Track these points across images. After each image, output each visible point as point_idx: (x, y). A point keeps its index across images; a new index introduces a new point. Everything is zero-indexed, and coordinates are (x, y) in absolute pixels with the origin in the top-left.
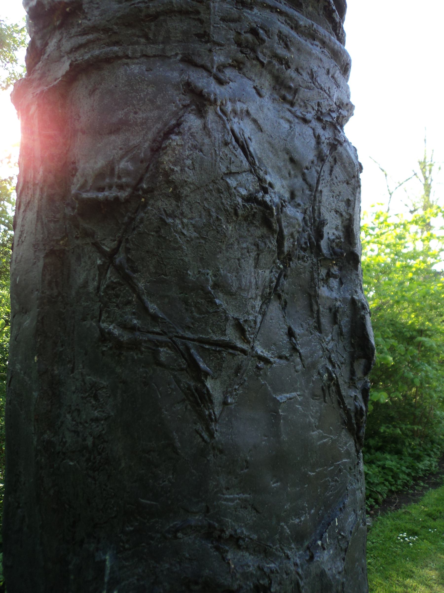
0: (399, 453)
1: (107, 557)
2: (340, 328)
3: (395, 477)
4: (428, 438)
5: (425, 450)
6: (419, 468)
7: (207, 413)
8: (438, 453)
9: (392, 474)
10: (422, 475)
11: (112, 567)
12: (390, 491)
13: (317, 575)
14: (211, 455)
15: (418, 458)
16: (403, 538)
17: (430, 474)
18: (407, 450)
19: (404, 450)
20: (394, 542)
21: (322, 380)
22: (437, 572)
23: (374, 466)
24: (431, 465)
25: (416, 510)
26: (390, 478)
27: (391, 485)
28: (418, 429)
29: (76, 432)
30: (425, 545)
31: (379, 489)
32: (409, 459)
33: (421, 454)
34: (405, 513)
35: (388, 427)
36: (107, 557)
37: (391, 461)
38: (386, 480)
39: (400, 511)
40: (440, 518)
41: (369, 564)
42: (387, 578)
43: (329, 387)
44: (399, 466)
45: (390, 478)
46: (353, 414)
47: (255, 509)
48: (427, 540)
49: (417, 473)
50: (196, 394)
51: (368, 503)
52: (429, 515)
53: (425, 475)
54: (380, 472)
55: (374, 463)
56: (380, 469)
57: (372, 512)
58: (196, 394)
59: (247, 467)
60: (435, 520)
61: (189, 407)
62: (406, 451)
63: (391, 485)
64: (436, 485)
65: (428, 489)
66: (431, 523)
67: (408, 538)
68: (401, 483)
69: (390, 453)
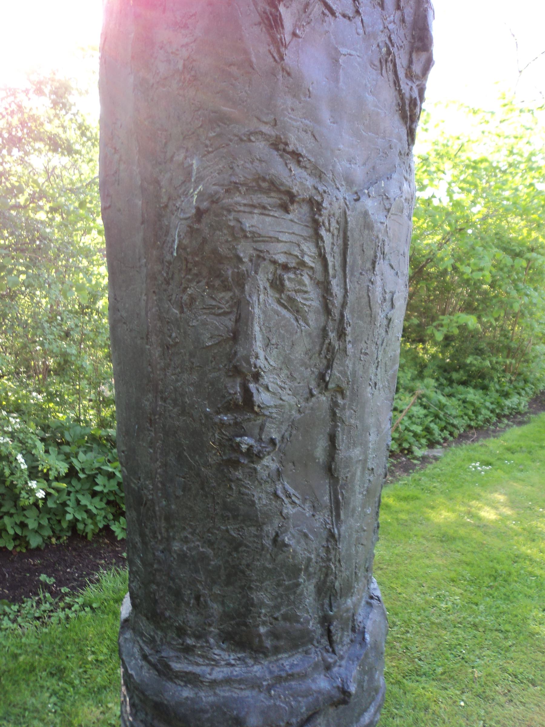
0: (485, 388)
1: (194, 162)
2: (403, 15)
3: (476, 412)
4: (522, 376)
5: (515, 388)
6: (505, 405)
7: (279, 36)
8: (531, 393)
9: (473, 408)
10: (508, 413)
11: (198, 169)
12: (470, 427)
13: (362, 212)
14: (281, 75)
15: (506, 395)
16: (475, 467)
17: (517, 413)
18: (494, 387)
19: (492, 384)
20: (465, 470)
21: (380, 51)
22: (506, 497)
23: (453, 399)
24: (520, 403)
25: (494, 444)
26: (470, 413)
27: (471, 420)
28: (511, 363)
29: (169, 61)
30: (500, 473)
31: (456, 422)
32: (495, 395)
33: (511, 391)
34: (481, 446)
35: (476, 359)
36: (194, 162)
37: (472, 395)
38: (466, 414)
39: (476, 444)
40: (520, 452)
41: (435, 487)
42: (451, 499)
43: (386, 61)
44: (482, 401)
45: (470, 413)
46: (407, 102)
47: (314, 136)
48: (501, 469)
49: (503, 410)
50: (271, 17)
51: (442, 434)
52: (508, 449)
53: (511, 414)
54: (459, 406)
55: (454, 396)
56: (460, 402)
57: (445, 445)
58: (271, 17)
59: (310, 97)
60: (513, 453)
61: (264, 29)
62: (493, 386)
63: (471, 420)
64: (521, 423)
65: (512, 426)
66: (508, 455)
67: (481, 467)
68: (483, 419)
69: (475, 387)
